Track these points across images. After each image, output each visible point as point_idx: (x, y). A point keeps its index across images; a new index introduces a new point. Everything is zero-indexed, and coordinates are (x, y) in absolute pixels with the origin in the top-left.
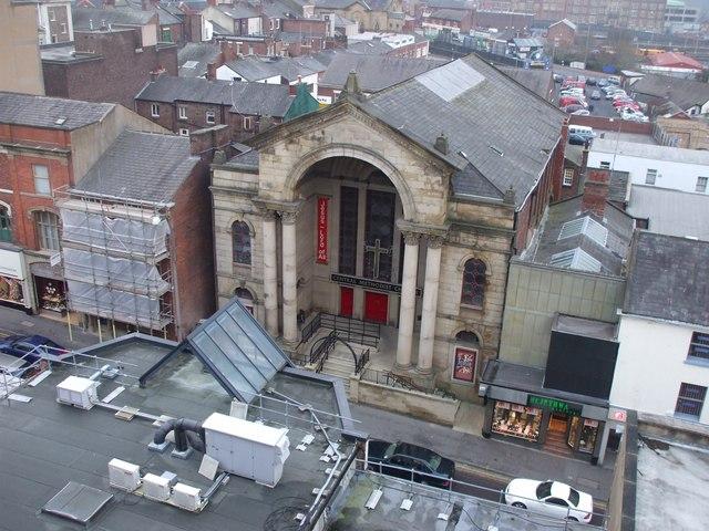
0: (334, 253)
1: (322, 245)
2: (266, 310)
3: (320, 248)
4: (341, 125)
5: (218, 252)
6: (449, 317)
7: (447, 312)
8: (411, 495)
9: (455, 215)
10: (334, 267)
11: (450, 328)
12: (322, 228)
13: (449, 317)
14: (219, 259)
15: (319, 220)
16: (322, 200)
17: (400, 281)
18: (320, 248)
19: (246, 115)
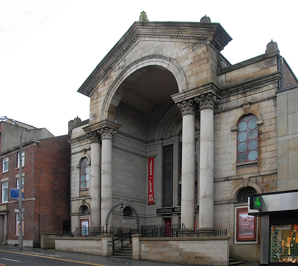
0: (158, 194)
1: (151, 191)
2: (5, 214)
3: (150, 193)
4: (135, 48)
5: (72, 184)
6: (227, 179)
7: (225, 175)
8: (292, 77)
9: (237, 253)
10: (159, 204)
11: (228, 190)
12: (151, 178)
13: (227, 179)
14: (72, 188)
15: (149, 173)
16: (151, 159)
17: (180, 204)
18: (150, 193)
19: (178, 183)
